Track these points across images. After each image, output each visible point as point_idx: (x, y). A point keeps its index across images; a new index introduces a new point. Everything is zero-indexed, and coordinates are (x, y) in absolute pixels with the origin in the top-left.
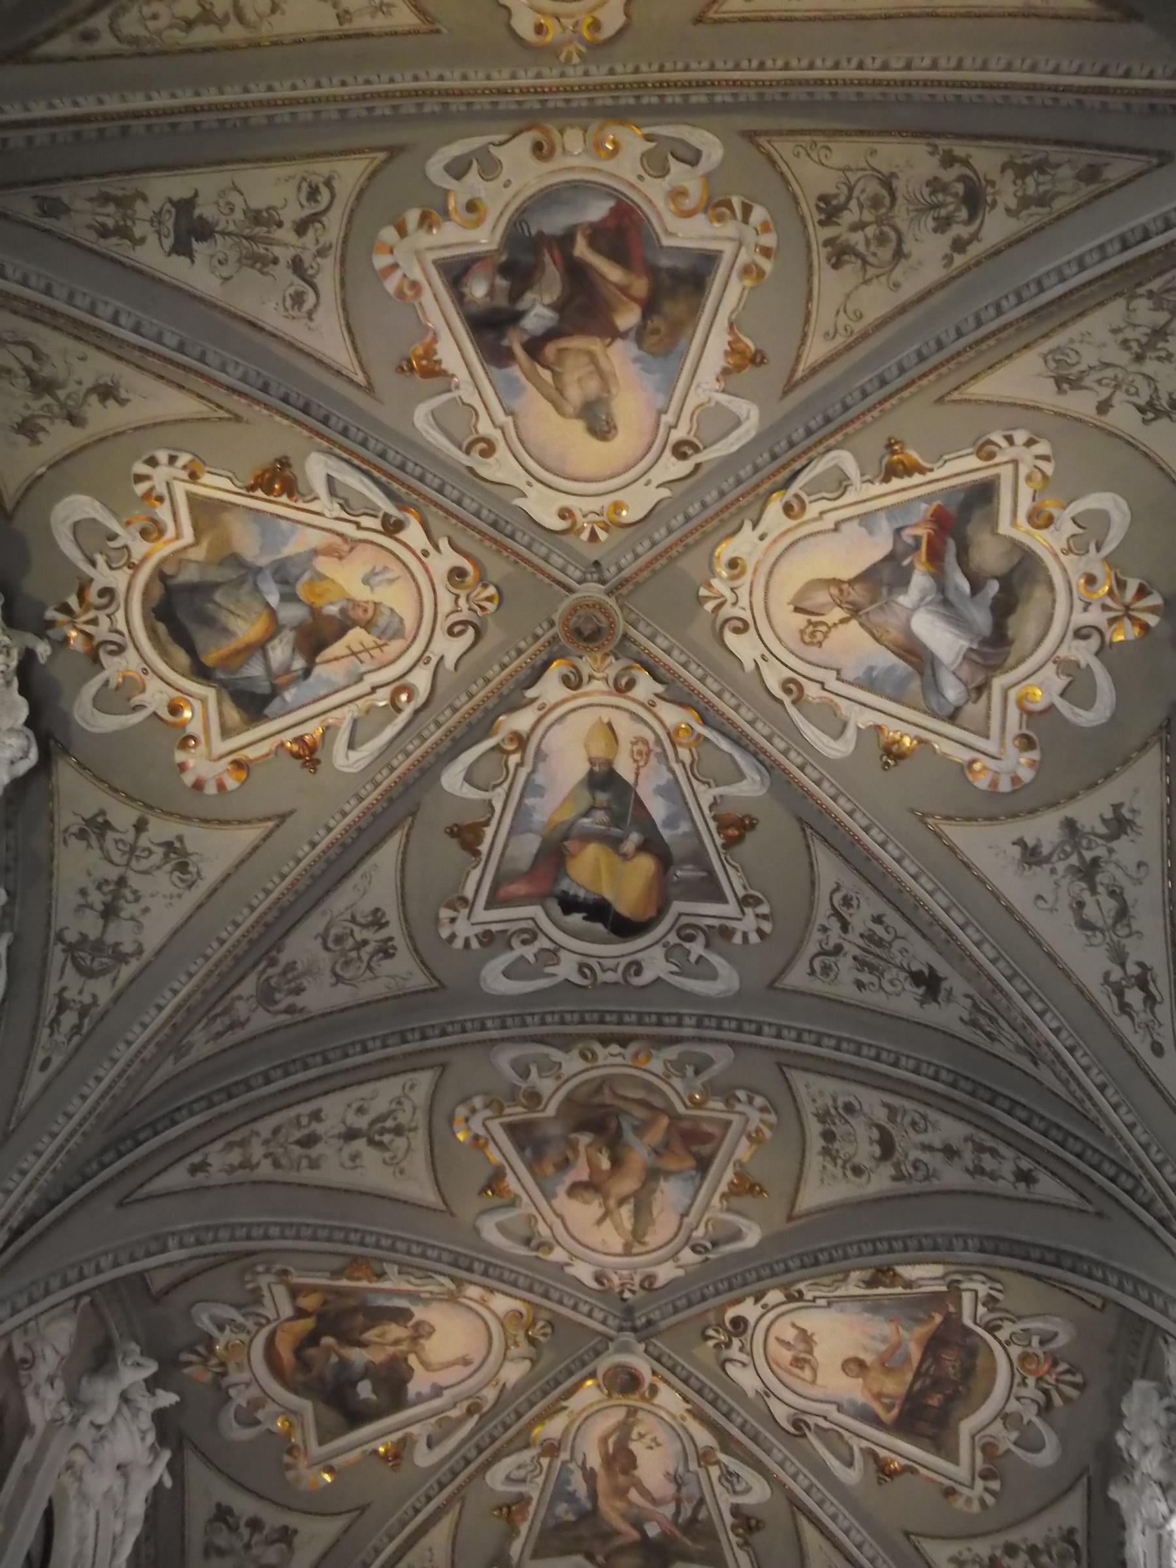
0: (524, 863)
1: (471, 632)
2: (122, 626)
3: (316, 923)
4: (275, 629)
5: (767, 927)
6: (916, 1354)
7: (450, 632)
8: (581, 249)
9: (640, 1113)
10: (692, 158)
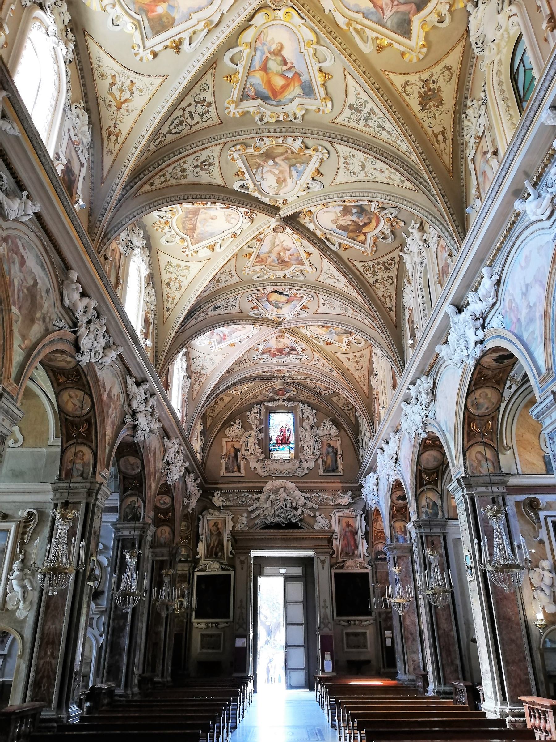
6: (198, 224)
9: (272, 264)
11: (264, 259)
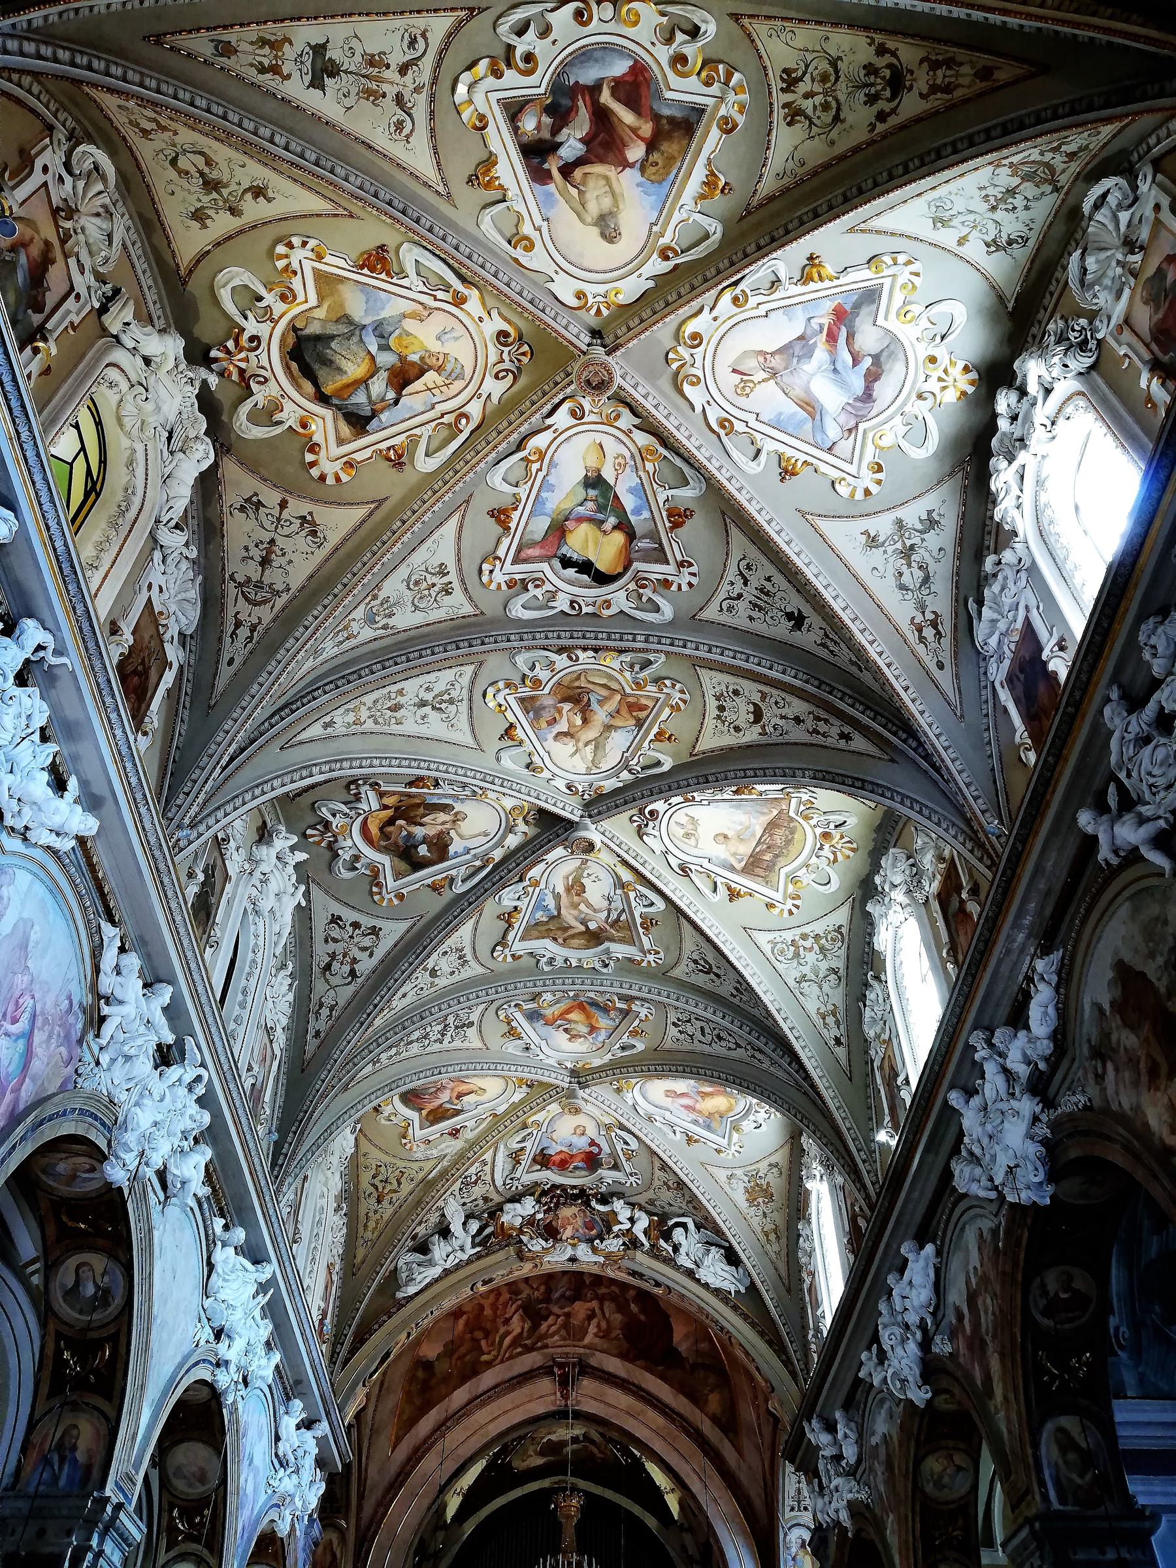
0: (539, 536)
1: (511, 376)
2: (266, 364)
3: (403, 572)
4: (374, 371)
5: (695, 581)
7: (497, 377)
8: (606, 97)
9: (605, 692)
10: (694, 32)
11: (624, 711)
